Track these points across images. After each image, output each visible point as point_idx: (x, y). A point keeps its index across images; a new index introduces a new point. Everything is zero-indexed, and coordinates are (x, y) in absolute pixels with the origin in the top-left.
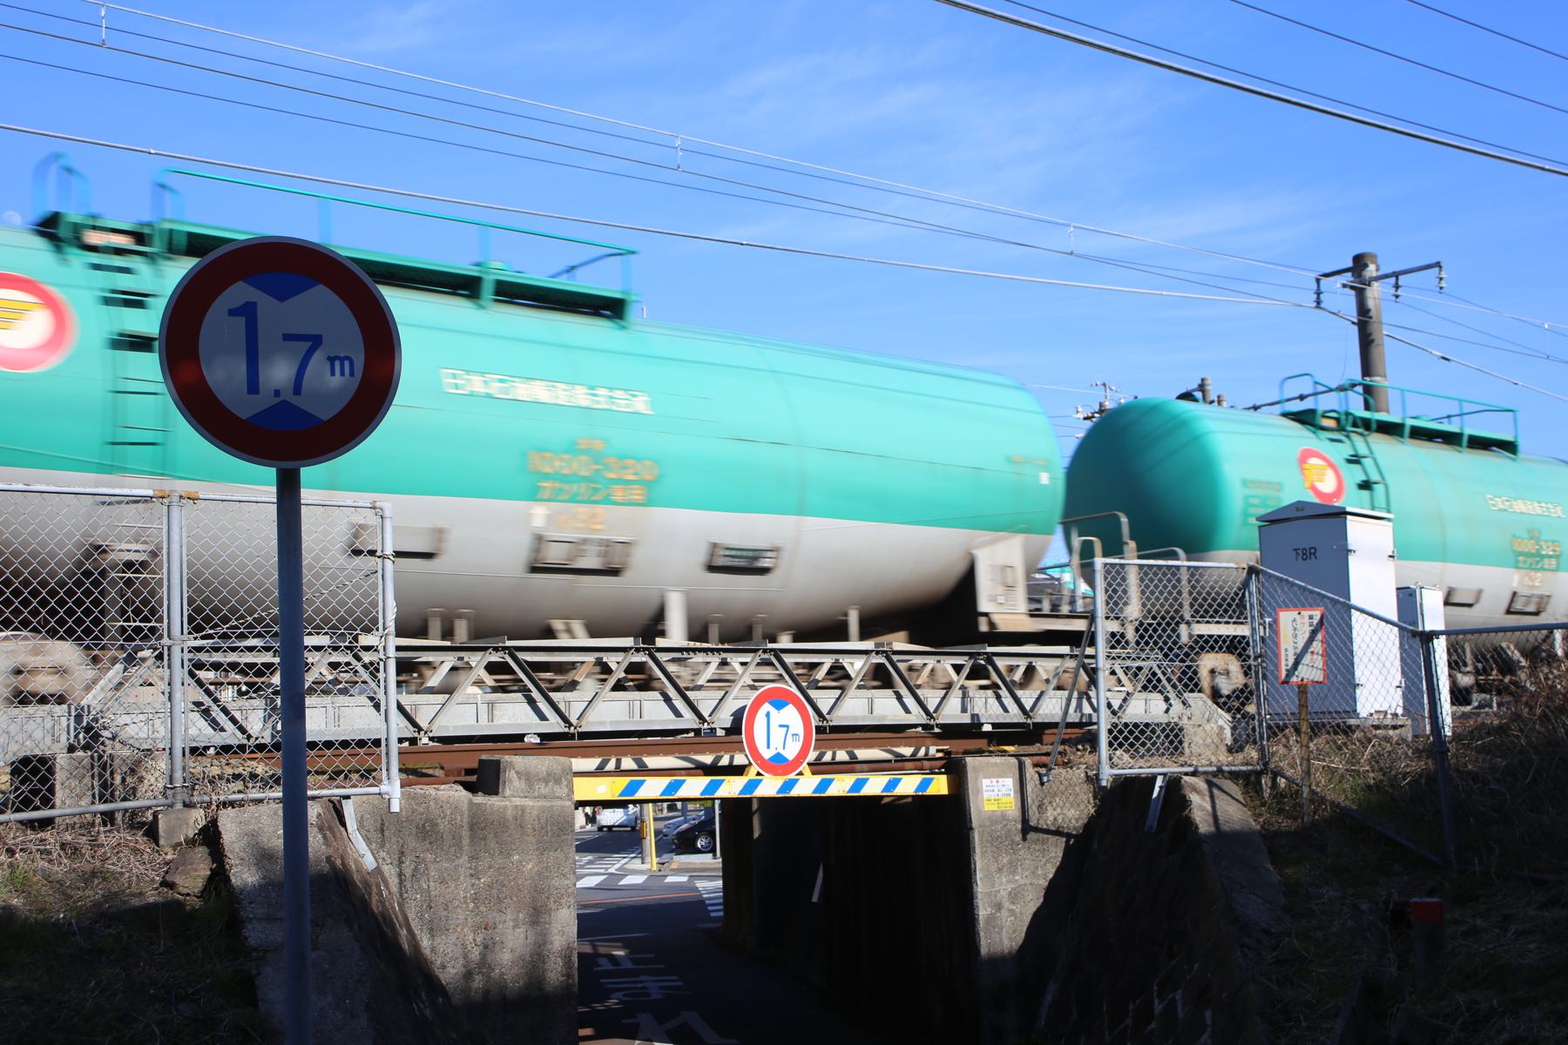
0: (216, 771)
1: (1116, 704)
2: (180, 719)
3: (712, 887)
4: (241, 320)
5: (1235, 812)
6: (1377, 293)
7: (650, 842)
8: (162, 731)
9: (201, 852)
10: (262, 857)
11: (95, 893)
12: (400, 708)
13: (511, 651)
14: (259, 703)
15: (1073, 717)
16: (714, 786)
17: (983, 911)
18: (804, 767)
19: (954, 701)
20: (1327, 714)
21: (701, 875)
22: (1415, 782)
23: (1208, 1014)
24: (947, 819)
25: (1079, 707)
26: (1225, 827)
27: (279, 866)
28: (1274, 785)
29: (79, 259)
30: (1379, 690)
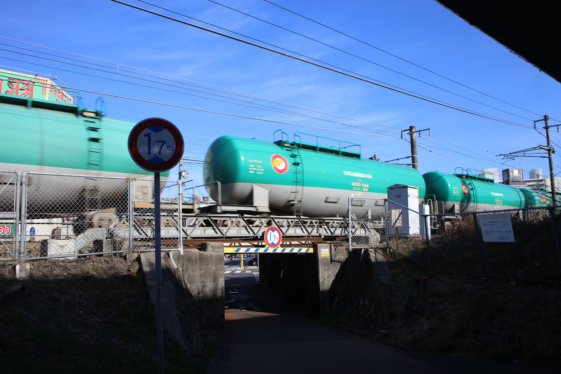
0: (140, 244)
1: (353, 232)
2: (132, 232)
3: (256, 274)
4: (147, 137)
5: (380, 257)
6: (415, 135)
7: (242, 263)
8: (127, 235)
9: (136, 263)
10: (151, 264)
11: (112, 272)
12: (183, 230)
13: (209, 217)
14: (150, 228)
15: (343, 234)
16: (257, 250)
17: (321, 280)
18: (279, 246)
19: (315, 231)
20: (402, 234)
21: (254, 271)
22: (422, 250)
23: (373, 304)
24: (313, 258)
25: (345, 232)
26: (378, 261)
27: (154, 267)
28: (390, 251)
29: (81, 119)
30: (414, 229)
